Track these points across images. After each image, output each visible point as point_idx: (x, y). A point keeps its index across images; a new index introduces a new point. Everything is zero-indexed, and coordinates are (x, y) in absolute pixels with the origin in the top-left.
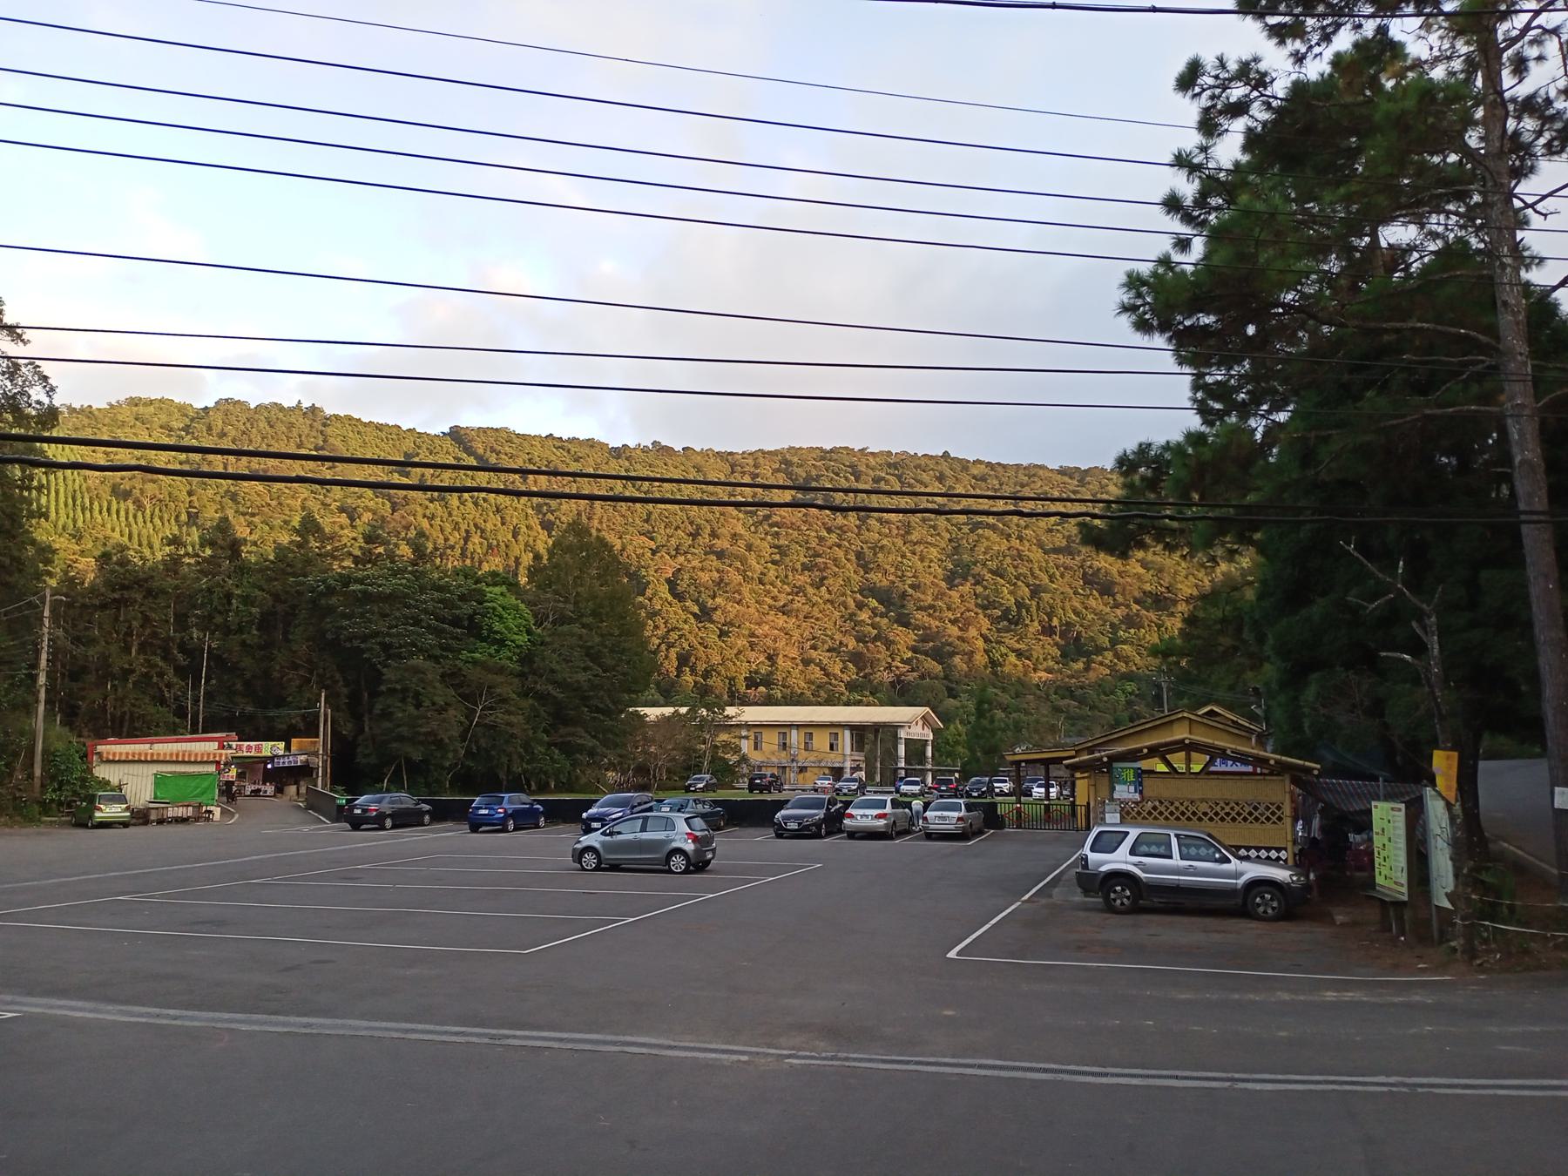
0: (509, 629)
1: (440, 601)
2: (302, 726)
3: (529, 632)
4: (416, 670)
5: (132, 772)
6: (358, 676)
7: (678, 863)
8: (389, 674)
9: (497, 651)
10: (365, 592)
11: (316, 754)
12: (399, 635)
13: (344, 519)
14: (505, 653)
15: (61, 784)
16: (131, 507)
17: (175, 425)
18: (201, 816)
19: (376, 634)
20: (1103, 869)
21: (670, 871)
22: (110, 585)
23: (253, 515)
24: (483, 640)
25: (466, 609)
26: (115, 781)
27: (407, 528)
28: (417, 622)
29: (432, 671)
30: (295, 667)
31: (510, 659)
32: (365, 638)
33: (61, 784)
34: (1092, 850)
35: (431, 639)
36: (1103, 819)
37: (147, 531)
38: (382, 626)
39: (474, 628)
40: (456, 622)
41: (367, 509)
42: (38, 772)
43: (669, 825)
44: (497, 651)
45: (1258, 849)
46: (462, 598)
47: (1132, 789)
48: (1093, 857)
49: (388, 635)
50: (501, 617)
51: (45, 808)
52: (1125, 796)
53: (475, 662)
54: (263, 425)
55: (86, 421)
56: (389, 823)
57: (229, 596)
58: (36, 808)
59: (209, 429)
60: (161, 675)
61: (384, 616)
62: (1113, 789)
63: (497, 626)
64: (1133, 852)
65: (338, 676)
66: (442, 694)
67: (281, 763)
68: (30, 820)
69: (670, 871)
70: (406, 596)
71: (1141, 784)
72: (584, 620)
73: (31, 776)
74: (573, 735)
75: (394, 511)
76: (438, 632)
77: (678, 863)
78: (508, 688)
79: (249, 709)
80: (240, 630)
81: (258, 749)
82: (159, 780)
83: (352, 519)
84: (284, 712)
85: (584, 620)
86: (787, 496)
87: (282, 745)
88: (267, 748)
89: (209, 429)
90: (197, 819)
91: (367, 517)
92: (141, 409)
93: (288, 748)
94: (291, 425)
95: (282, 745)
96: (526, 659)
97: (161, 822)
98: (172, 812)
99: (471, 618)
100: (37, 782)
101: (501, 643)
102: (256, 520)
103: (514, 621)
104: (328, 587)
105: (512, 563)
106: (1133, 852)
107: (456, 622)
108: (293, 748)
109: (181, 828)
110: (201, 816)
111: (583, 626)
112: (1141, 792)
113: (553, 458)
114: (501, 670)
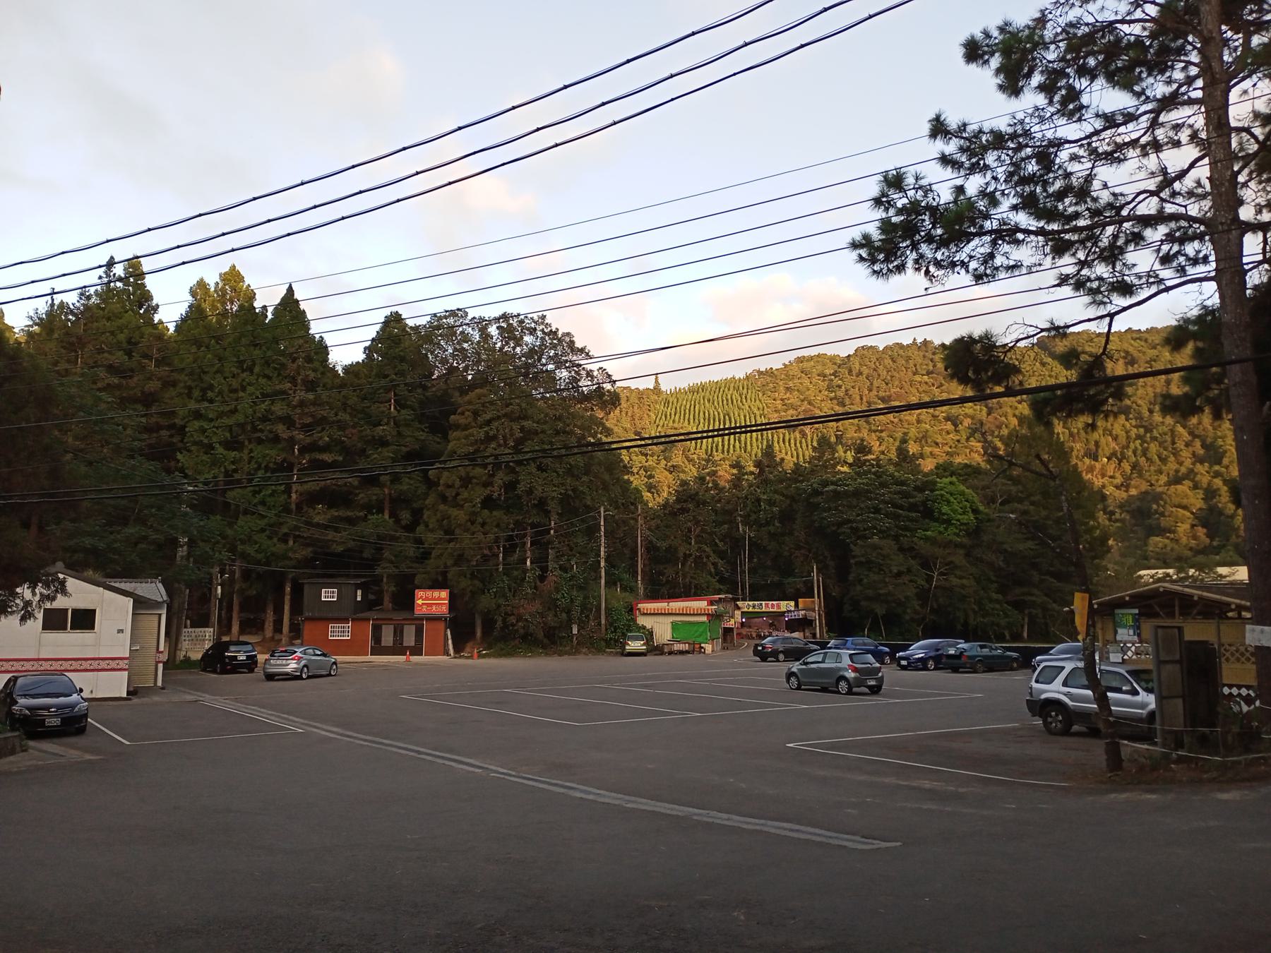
0: (954, 511)
1: (899, 493)
2: (803, 590)
3: (975, 511)
4: (875, 547)
5: (660, 620)
6: (837, 551)
7: (843, 686)
8: (857, 551)
9: (946, 529)
10: (835, 491)
11: (814, 610)
12: (864, 521)
13: (949, 426)
14: (952, 530)
15: (616, 629)
16: (798, 436)
17: (827, 372)
18: (695, 649)
19: (849, 521)
20: (1043, 696)
21: (839, 692)
22: (678, 501)
23: (881, 431)
24: (936, 520)
25: (919, 497)
26: (649, 627)
27: (999, 427)
28: (877, 511)
29: (889, 545)
30: (799, 548)
31: (958, 535)
32: (840, 525)
33: (616, 629)
34: (1037, 681)
35: (888, 523)
36: (1108, 658)
37: (687, 464)
38: (851, 515)
39: (928, 513)
40: (913, 508)
41: (966, 416)
42: (603, 622)
43: (838, 658)
44: (946, 529)
45: (1239, 687)
46: (917, 489)
47: (1131, 632)
48: (1035, 685)
49: (854, 521)
50: (948, 502)
51: (608, 645)
52: (1126, 638)
53: (927, 539)
54: (888, 361)
55: (769, 379)
56: (781, 657)
57: (758, 500)
58: (603, 643)
59: (850, 371)
60: (708, 557)
61: (851, 507)
62: (1116, 632)
63: (945, 509)
64: (1065, 684)
65: (826, 554)
66: (897, 562)
67: (794, 616)
68: (600, 651)
69: (839, 692)
70: (868, 491)
71: (1139, 628)
72: (1032, 498)
73: (600, 624)
74: (1032, 595)
75: (989, 414)
76: (896, 517)
77: (843, 686)
78: (959, 558)
79: (776, 578)
80: (768, 524)
81: (778, 606)
82: (674, 625)
83: (956, 425)
84: (791, 580)
85: (1032, 498)
86: (614, 446)
87: (792, 603)
88: (785, 605)
89: (850, 371)
90: (693, 652)
91: (967, 422)
92: (805, 365)
93: (797, 605)
94: (908, 358)
95: (792, 603)
96: (975, 533)
97: (670, 653)
98: (677, 647)
99: (924, 503)
100: (603, 628)
101: (948, 522)
102: (883, 434)
103: (959, 503)
104: (813, 490)
105: (1092, 446)
106: (1065, 684)
107: (913, 508)
108: (800, 606)
109: (680, 657)
110: (695, 649)
111: (1032, 503)
112: (1139, 635)
113: (1131, 349)
114: (947, 544)
